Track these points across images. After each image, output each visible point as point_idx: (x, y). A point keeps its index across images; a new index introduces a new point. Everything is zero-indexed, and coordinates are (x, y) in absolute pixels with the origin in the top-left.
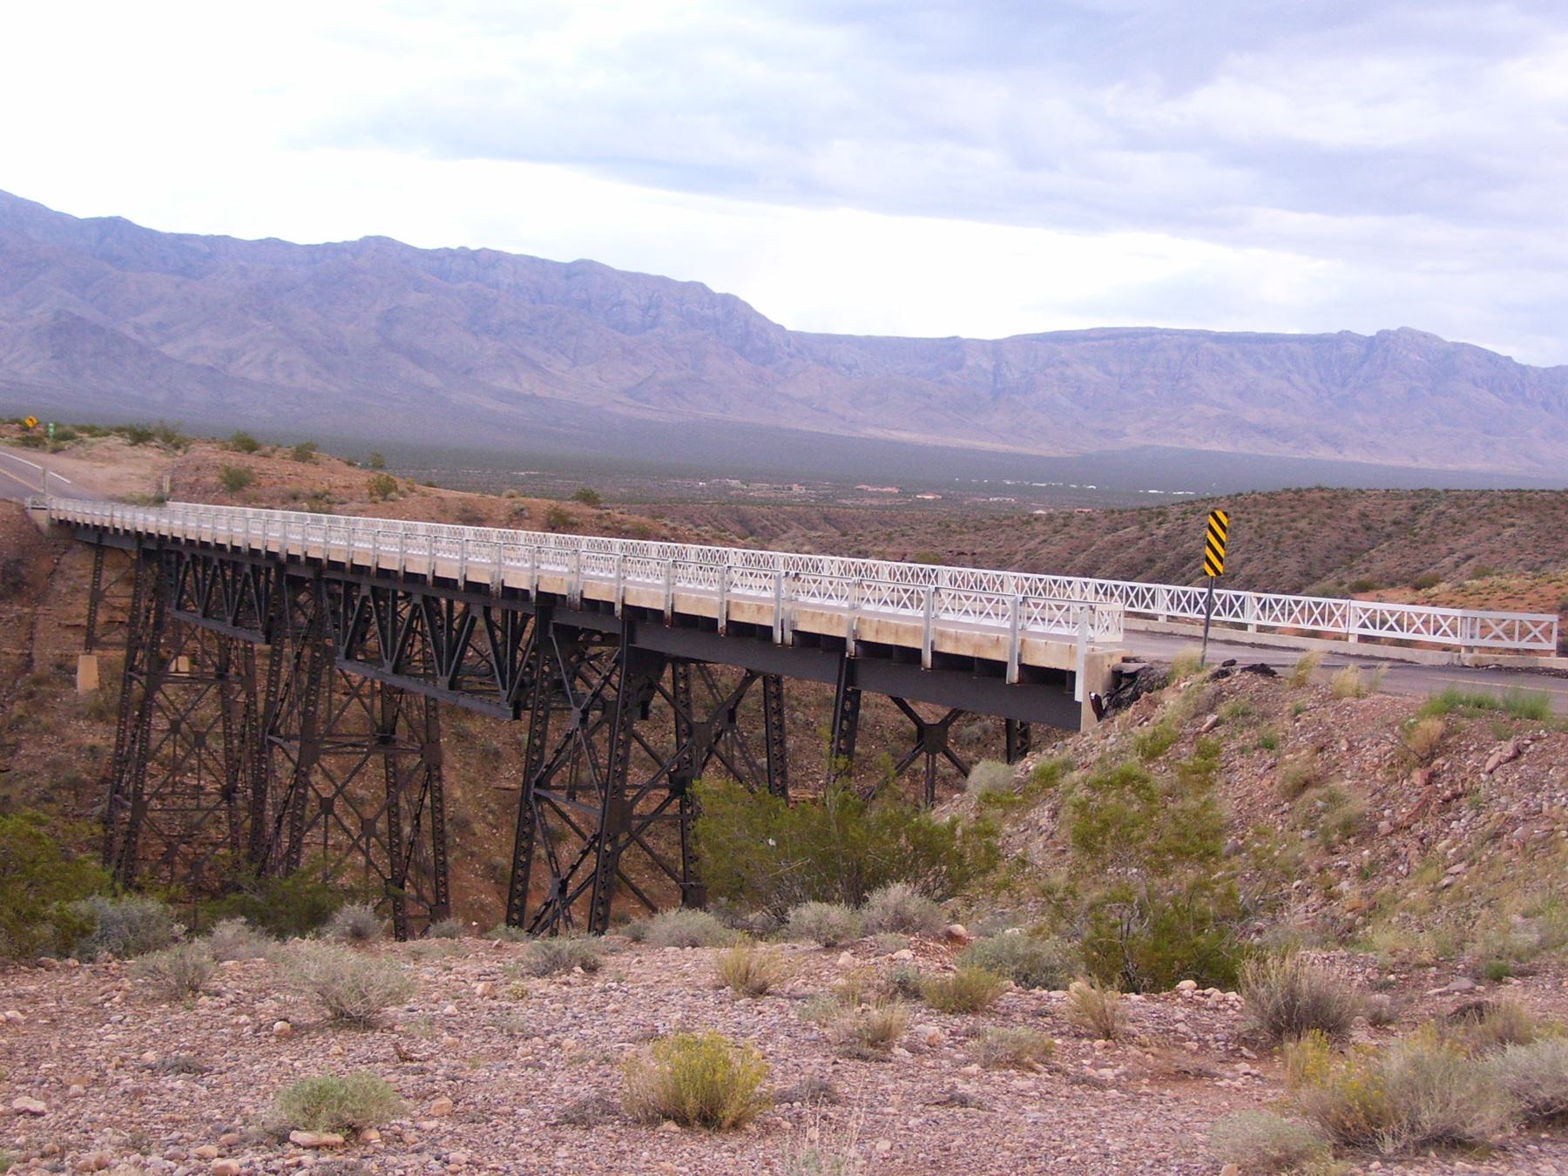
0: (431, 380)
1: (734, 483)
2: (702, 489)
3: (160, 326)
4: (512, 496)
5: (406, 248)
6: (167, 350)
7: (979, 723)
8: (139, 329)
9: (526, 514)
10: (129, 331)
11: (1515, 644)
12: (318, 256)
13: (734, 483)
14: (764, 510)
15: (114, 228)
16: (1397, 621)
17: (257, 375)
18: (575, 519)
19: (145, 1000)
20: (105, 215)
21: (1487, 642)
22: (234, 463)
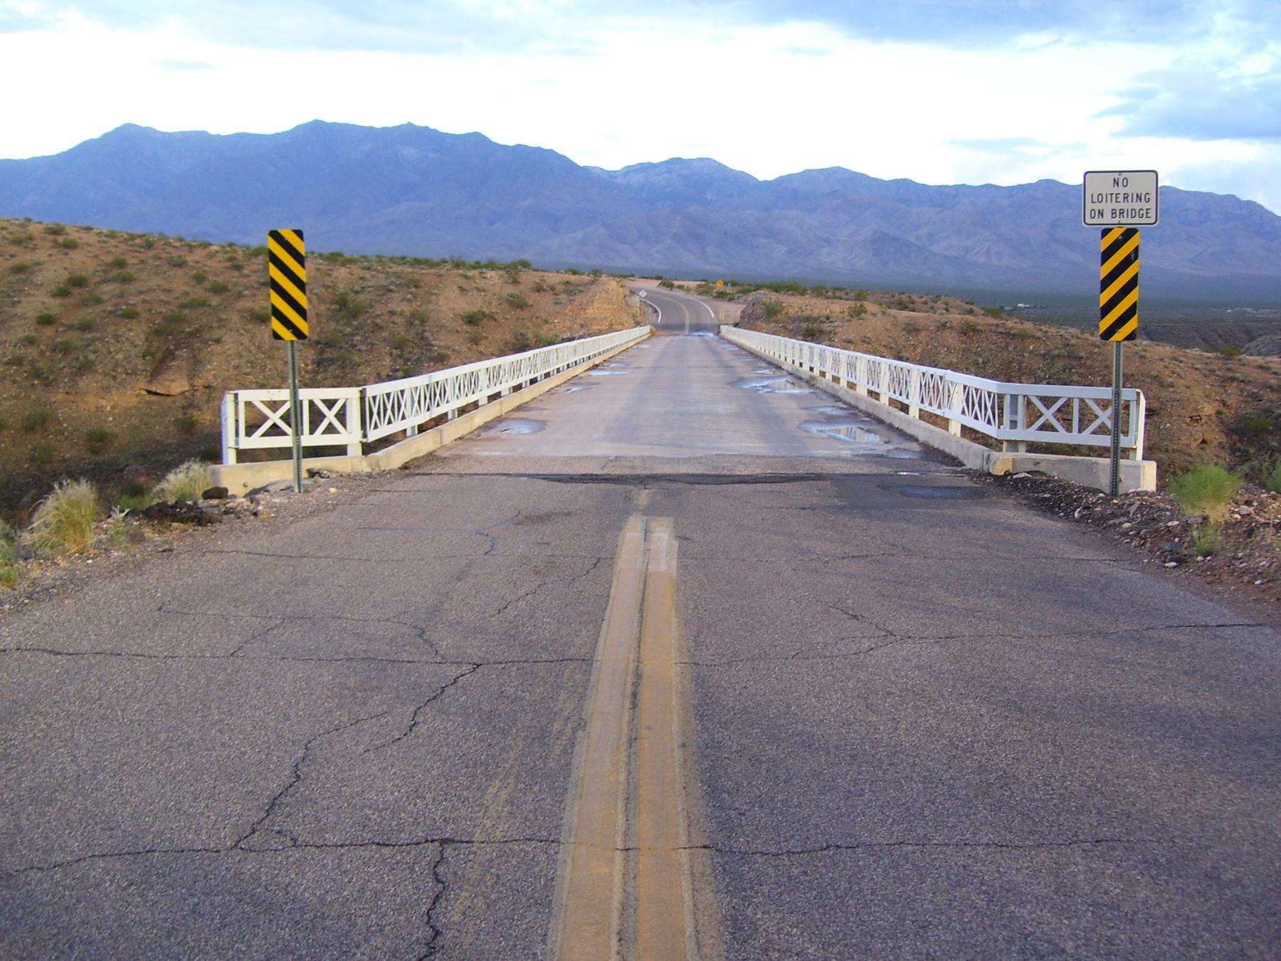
0: (1077, 258)
1: (1248, 310)
2: (1229, 313)
3: (930, 236)
4: (942, 314)
5: (369, 132)
6: (934, 248)
7: (1248, 463)
8: (918, 238)
9: (948, 325)
10: (912, 239)
11: (1074, 438)
12: (1014, 193)
13: (1248, 310)
14: (1261, 325)
15: (904, 186)
16: (322, 416)
17: (981, 260)
18: (980, 327)
19: (855, 576)
20: (899, 178)
21: (1034, 435)
22: (773, 300)
